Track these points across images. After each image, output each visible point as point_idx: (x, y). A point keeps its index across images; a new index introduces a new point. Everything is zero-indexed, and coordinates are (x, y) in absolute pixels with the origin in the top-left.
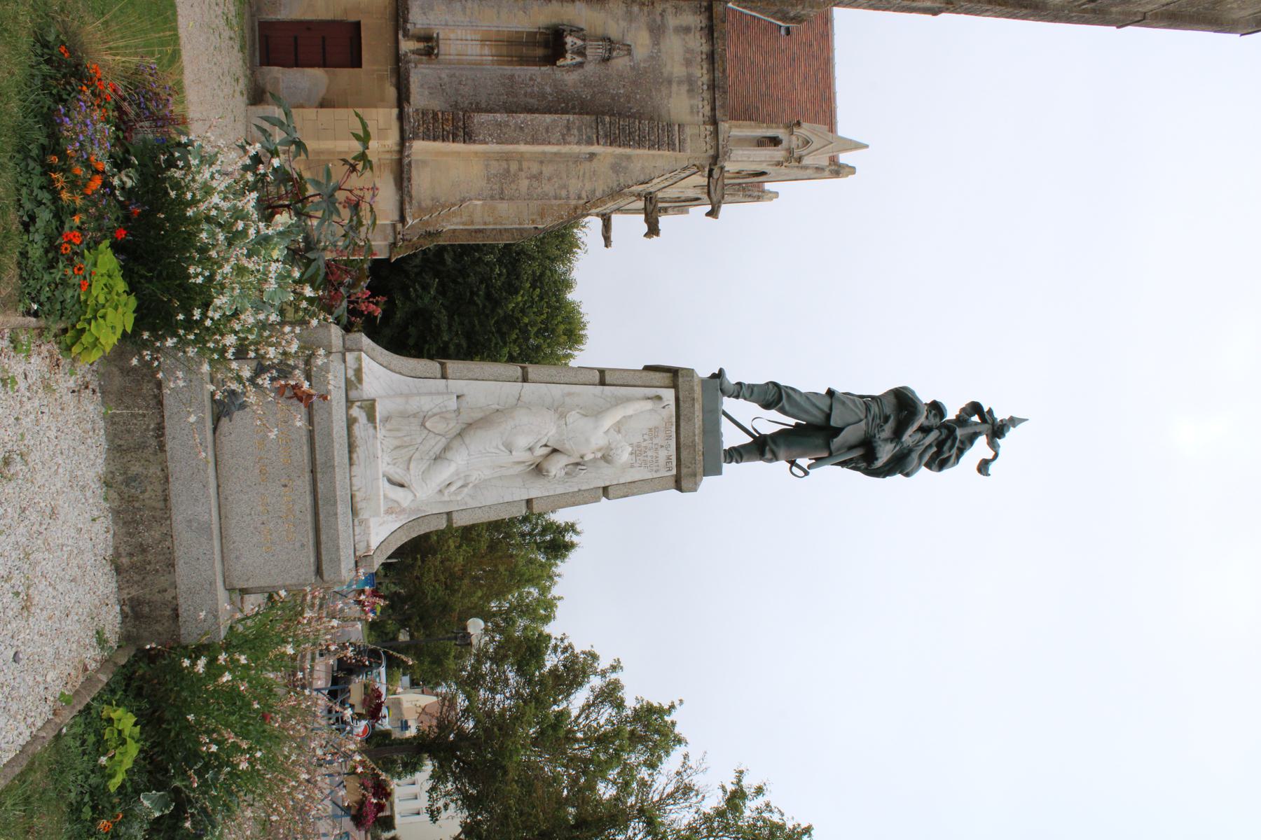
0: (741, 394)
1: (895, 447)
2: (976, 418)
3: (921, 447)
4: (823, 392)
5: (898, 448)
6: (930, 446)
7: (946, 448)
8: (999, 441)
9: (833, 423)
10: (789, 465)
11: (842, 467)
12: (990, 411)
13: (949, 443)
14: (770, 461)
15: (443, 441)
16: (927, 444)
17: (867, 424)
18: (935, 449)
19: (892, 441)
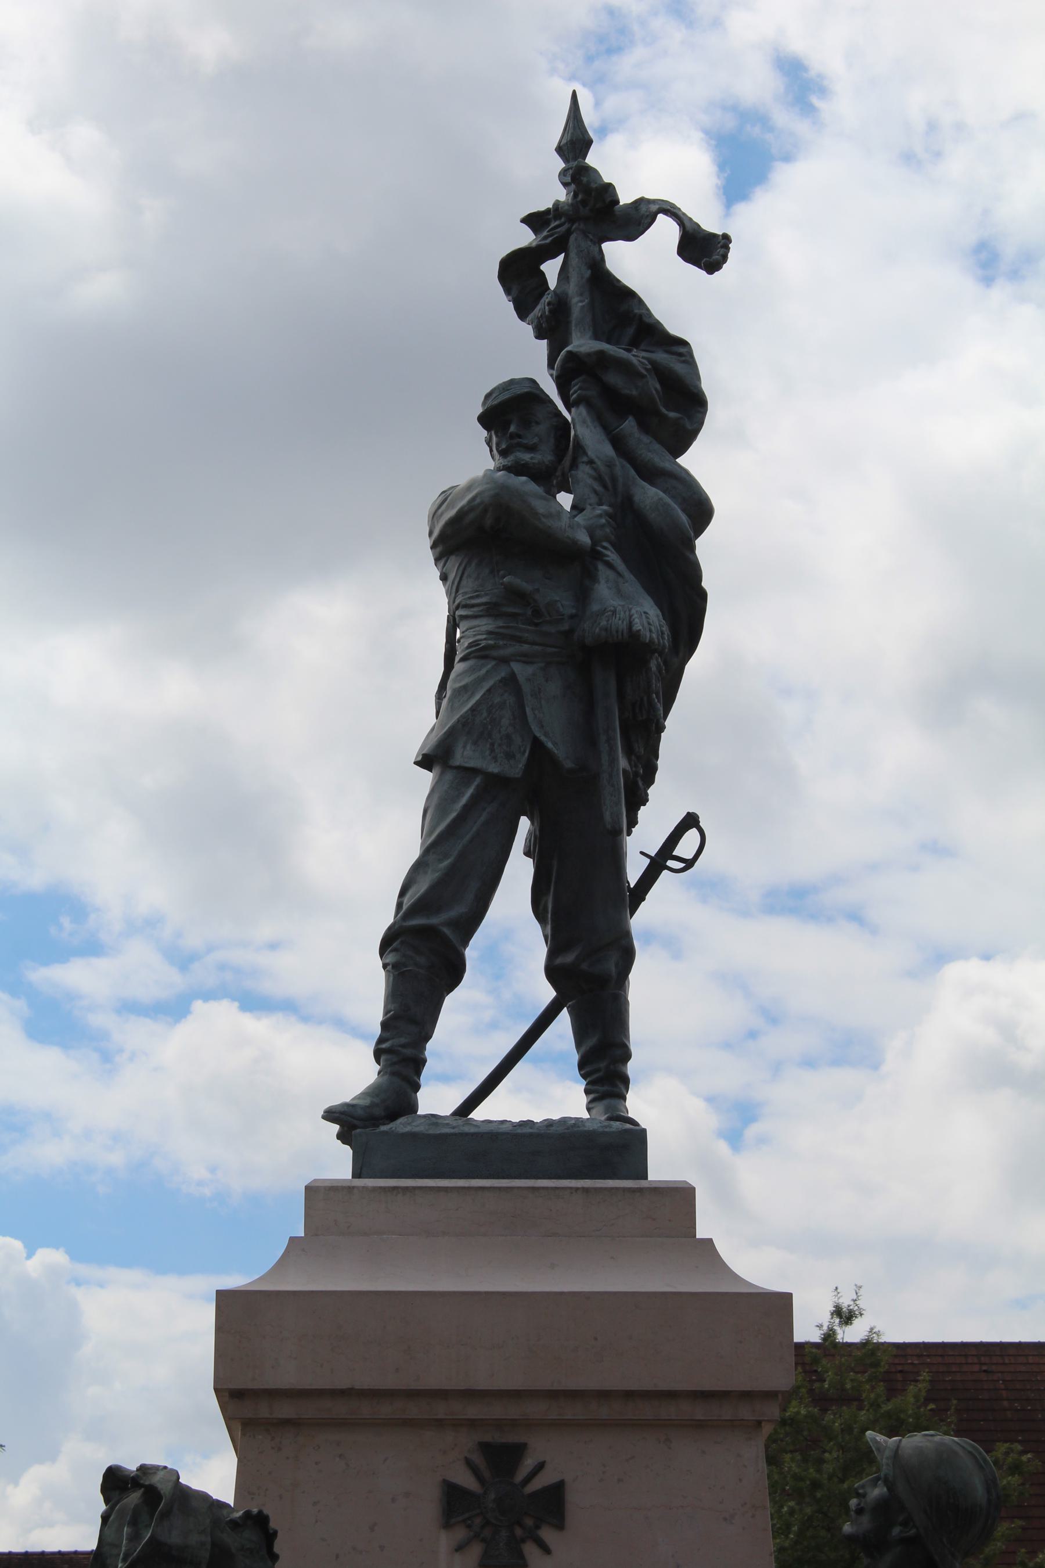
0: (408, 1052)
1: (610, 565)
2: (551, 269)
3: (618, 471)
4: (426, 778)
5: (612, 556)
6: (617, 442)
7: (632, 391)
8: (626, 197)
9: (516, 769)
10: (665, 872)
11: (644, 801)
12: (534, 221)
13: (614, 379)
14: (582, 1075)
15: (176, 980)
16: (608, 450)
17: (526, 659)
18: (629, 425)
19: (590, 576)
